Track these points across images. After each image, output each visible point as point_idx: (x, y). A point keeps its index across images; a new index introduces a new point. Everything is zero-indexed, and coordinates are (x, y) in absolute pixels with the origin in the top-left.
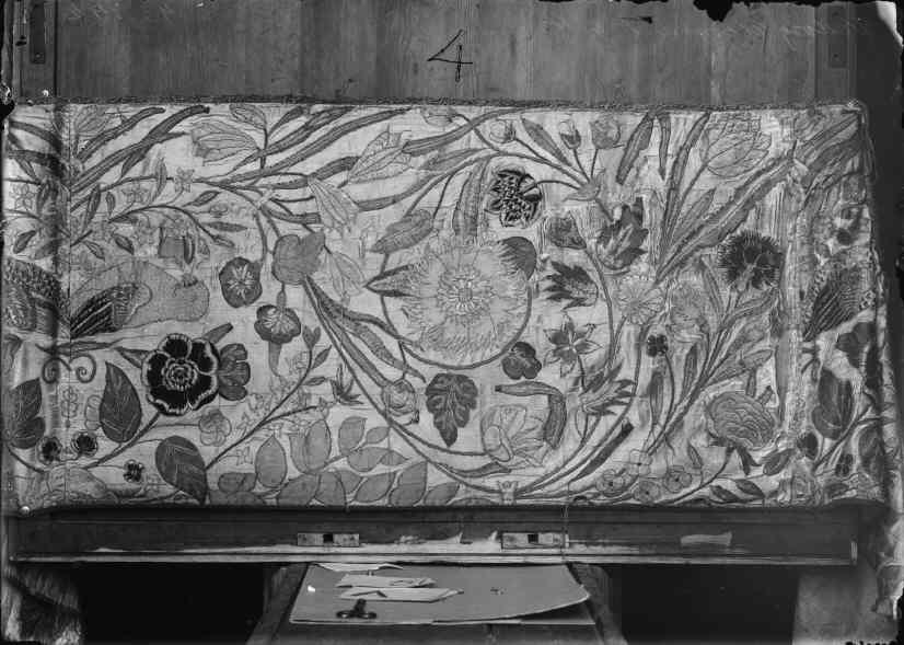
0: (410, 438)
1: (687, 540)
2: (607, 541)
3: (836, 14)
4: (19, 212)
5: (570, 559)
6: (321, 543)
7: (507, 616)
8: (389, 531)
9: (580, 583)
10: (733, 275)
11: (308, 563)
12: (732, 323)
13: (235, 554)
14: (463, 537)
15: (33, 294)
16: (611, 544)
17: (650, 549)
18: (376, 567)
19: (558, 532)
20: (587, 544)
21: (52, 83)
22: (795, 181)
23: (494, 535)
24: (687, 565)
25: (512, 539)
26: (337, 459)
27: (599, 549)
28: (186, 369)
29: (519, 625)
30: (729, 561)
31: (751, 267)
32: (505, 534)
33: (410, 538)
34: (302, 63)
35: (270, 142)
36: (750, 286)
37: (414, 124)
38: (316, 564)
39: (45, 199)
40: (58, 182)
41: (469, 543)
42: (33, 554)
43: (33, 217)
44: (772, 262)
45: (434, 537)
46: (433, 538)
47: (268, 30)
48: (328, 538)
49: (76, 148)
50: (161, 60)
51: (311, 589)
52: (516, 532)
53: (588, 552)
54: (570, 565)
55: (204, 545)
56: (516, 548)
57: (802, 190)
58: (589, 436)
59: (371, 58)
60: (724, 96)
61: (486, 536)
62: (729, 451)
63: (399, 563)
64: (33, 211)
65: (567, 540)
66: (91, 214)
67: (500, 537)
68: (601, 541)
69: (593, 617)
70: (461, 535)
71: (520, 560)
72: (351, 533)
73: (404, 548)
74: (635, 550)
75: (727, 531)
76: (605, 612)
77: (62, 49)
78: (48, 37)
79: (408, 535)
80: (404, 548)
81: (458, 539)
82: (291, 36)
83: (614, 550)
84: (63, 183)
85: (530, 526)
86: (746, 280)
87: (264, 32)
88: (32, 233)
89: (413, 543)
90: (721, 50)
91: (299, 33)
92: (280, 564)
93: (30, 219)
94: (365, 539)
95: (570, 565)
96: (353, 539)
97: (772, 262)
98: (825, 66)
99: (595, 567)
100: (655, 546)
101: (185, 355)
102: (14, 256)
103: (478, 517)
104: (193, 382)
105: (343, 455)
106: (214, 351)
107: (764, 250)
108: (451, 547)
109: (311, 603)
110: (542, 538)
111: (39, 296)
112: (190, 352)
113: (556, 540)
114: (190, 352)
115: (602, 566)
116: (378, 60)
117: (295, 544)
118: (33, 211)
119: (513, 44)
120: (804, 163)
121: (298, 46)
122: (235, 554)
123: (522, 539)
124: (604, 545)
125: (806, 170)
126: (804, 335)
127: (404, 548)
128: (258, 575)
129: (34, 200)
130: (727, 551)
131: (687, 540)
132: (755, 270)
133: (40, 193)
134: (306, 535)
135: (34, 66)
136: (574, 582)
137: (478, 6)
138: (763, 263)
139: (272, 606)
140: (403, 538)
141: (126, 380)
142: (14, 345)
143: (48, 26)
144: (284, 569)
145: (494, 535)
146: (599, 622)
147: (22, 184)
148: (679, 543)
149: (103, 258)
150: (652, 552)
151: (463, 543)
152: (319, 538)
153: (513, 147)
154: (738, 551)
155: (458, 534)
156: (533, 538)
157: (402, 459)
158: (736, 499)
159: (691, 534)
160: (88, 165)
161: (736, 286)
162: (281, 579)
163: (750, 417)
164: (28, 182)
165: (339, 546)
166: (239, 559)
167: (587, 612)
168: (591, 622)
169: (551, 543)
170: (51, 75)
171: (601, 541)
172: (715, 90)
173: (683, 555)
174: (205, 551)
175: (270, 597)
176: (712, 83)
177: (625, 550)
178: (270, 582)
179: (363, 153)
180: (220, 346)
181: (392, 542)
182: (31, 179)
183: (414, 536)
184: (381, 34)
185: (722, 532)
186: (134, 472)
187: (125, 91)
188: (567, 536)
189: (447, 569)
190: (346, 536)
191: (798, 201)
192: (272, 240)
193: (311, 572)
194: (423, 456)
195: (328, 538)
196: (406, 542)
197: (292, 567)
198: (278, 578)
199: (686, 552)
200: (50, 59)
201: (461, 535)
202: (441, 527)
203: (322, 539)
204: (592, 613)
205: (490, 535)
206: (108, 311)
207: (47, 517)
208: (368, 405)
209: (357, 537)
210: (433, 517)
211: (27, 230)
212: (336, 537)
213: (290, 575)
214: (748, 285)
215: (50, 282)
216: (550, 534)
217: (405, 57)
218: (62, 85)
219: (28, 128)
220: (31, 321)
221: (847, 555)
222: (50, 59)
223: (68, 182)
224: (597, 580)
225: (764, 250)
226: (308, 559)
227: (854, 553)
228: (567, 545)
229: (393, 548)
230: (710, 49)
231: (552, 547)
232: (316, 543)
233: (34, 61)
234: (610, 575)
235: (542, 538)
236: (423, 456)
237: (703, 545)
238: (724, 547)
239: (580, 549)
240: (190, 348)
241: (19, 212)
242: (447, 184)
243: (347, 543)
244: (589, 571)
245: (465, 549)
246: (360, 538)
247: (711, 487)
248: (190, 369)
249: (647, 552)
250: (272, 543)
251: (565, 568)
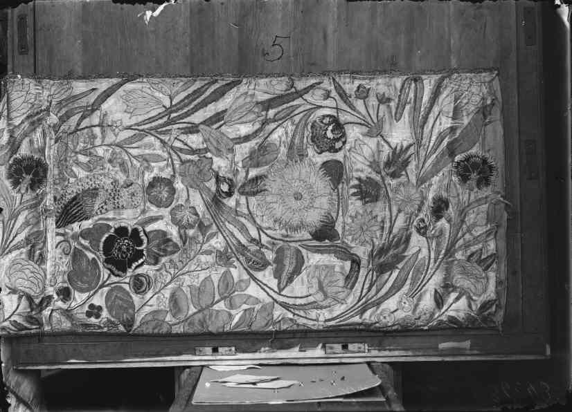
0: (265, 287)
1: (442, 346)
2: (392, 348)
5: (368, 360)
7: (330, 396)
8: (254, 345)
9: (376, 374)
10: (16, 183)
11: (203, 366)
12: (19, 213)
16: (394, 350)
18: (245, 368)
19: (361, 343)
20: (379, 350)
22: (49, 126)
23: (320, 345)
25: (331, 348)
26: (217, 302)
27: (387, 353)
29: (341, 402)
30: (469, 358)
31: (29, 177)
32: (327, 345)
33: (267, 348)
35: (173, 103)
36: (29, 190)
37: (263, 88)
38: (207, 366)
42: (28, 364)
44: (42, 175)
47: (170, 30)
48: (215, 350)
50: (102, 51)
51: (208, 385)
54: (369, 363)
55: (136, 356)
56: (335, 353)
57: (53, 132)
58: (256, 282)
61: (314, 346)
62: (20, 298)
63: (260, 365)
65: (367, 347)
67: (324, 347)
69: (384, 396)
70: (299, 346)
71: (337, 361)
72: (230, 347)
73: (263, 355)
75: (468, 339)
76: (391, 393)
78: (29, 37)
80: (264, 355)
81: (297, 349)
82: (184, 34)
85: (342, 340)
86: (26, 185)
87: (167, 31)
89: (269, 351)
91: (189, 31)
92: (185, 367)
94: (239, 350)
95: (369, 363)
96: (230, 350)
97: (42, 175)
99: (385, 365)
101: (111, 235)
103: (309, 335)
105: (222, 299)
106: (144, 231)
107: (37, 166)
108: (293, 354)
109: (205, 392)
110: (351, 347)
113: (360, 348)
115: (390, 363)
116: (240, 48)
117: (195, 354)
119: (325, 37)
120: (56, 115)
121: (188, 41)
123: (338, 347)
124: (390, 350)
125: (58, 120)
126: (56, 223)
127: (263, 355)
128: (170, 374)
130: (468, 352)
131: (442, 346)
132: (31, 179)
134: (201, 349)
136: (371, 373)
138: (36, 174)
139: (180, 394)
142: (418, 229)
143: (29, 31)
144: (187, 370)
145: (320, 345)
146: (387, 399)
148: (438, 348)
150: (420, 354)
151: (300, 351)
152: (209, 350)
153: (329, 102)
154: (476, 352)
155: (297, 345)
156: (345, 347)
157: (257, 301)
158: (26, 328)
159: (444, 342)
161: (19, 190)
162: (186, 376)
163: (32, 274)
167: (380, 393)
168: (383, 399)
169: (356, 349)
170: (32, 61)
173: (440, 356)
177: (403, 353)
179: (230, 108)
180: (148, 229)
181: (255, 352)
186: (94, 311)
187: (79, 71)
188: (366, 345)
189: (306, 368)
190: (227, 349)
191: (51, 139)
192: (177, 163)
193: (205, 370)
194: (282, 295)
195: (215, 350)
196: (264, 351)
197: (193, 369)
198: (184, 376)
199: (443, 353)
200: (31, 52)
201: (299, 346)
202: (287, 342)
203: (211, 351)
204: (384, 394)
205: (317, 346)
209: (233, 349)
210: (281, 336)
212: (220, 350)
214: (27, 189)
216: (356, 344)
217: (257, 46)
221: (544, 353)
222: (31, 52)
225: (37, 166)
226: (203, 363)
227: (548, 352)
228: (367, 351)
229: (257, 355)
230: (450, 34)
231: (360, 352)
233: (21, 53)
234: (394, 369)
235: (351, 347)
236: (282, 295)
237: (453, 349)
238: (465, 349)
239: (374, 353)
242: (360, 124)
243: (227, 353)
244: (381, 367)
245: (302, 355)
246: (236, 350)
247: (10, 321)
249: (417, 353)
250: (180, 354)
251: (366, 365)
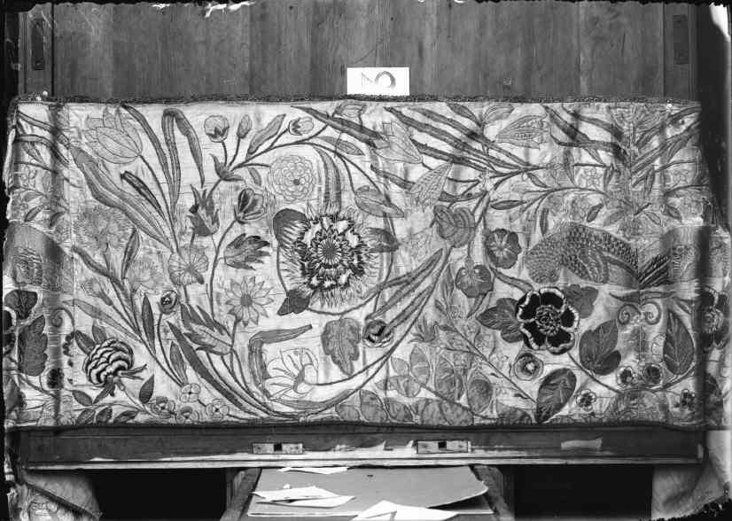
1: (566, 445)
2: (502, 446)
3: (679, 22)
4: (590, 190)
5: (472, 462)
6: (272, 451)
8: (327, 441)
11: (261, 468)
13: (203, 461)
14: (386, 446)
15: (606, 254)
16: (505, 449)
17: (536, 452)
20: (486, 450)
21: (50, 86)
23: (412, 442)
24: (566, 465)
25: (425, 446)
27: (496, 453)
28: (714, 316)
30: (600, 461)
33: (344, 446)
34: (251, 65)
39: (610, 178)
40: (621, 165)
41: (391, 450)
42: (41, 463)
43: (603, 193)
45: (363, 445)
46: (362, 446)
47: (223, 40)
48: (278, 448)
49: (634, 138)
52: (426, 440)
53: (488, 455)
54: (472, 467)
55: (178, 454)
56: (429, 453)
59: (308, 63)
60: (591, 88)
64: (601, 188)
65: (470, 446)
66: (648, 190)
67: (415, 445)
68: (497, 446)
69: (491, 508)
70: (384, 443)
71: (432, 463)
72: (297, 443)
74: (525, 454)
77: (59, 57)
79: (341, 444)
83: (508, 453)
84: (626, 166)
88: (600, 206)
90: (588, 51)
93: (600, 195)
94: (307, 448)
95: (472, 467)
96: (297, 448)
98: (671, 62)
100: (540, 451)
102: (587, 224)
103: (396, 430)
104: (719, 326)
108: (377, 453)
110: (450, 445)
111: (610, 255)
112: (716, 302)
113: (461, 447)
114: (716, 302)
115: (499, 467)
118: (601, 188)
122: (203, 461)
123: (434, 446)
124: (500, 450)
127: (338, 455)
129: (601, 180)
130: (598, 453)
131: (566, 445)
133: (606, 174)
134: (260, 445)
135: (36, 72)
137: (392, 19)
140: (338, 447)
141: (680, 323)
144: (242, 472)
145: (412, 442)
147: (591, 167)
149: (25, 221)
150: (538, 455)
151: (385, 450)
152: (270, 447)
156: (442, 445)
160: (644, 152)
164: (595, 166)
165: (287, 454)
166: (206, 465)
169: (456, 448)
170: (49, 80)
171: (497, 446)
172: (584, 84)
174: (180, 459)
175: (232, 495)
176: (581, 79)
177: (516, 454)
178: (232, 482)
182: (599, 164)
183: (347, 444)
184: (314, 41)
185: (595, 438)
190: (292, 446)
195: (278, 448)
196: (340, 450)
197: (249, 471)
198: (238, 480)
200: (48, 67)
201: (384, 443)
202: (368, 438)
204: (491, 505)
205: (408, 443)
206: (667, 268)
207: (52, 434)
208: (227, 335)
209: (301, 446)
210: (362, 429)
211: (597, 203)
212: (284, 447)
213: (248, 477)
215: (618, 244)
216: (457, 442)
218: (58, 88)
219: (593, 121)
220: (604, 275)
221: (695, 456)
223: (629, 165)
224: (494, 478)
226: (262, 464)
228: (469, 450)
231: (461, 451)
232: (268, 452)
233: (36, 68)
235: (450, 445)
238: (596, 450)
239: (480, 453)
240: (717, 298)
241: (590, 190)
245: (388, 454)
246: (304, 447)
248: (716, 316)
249: (534, 454)
250: (232, 452)
251: (468, 469)
